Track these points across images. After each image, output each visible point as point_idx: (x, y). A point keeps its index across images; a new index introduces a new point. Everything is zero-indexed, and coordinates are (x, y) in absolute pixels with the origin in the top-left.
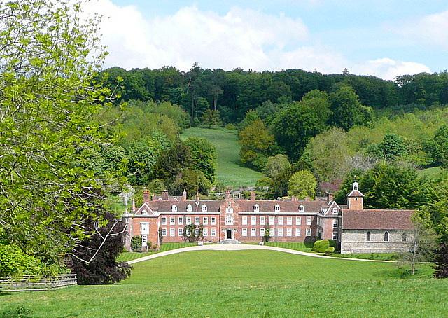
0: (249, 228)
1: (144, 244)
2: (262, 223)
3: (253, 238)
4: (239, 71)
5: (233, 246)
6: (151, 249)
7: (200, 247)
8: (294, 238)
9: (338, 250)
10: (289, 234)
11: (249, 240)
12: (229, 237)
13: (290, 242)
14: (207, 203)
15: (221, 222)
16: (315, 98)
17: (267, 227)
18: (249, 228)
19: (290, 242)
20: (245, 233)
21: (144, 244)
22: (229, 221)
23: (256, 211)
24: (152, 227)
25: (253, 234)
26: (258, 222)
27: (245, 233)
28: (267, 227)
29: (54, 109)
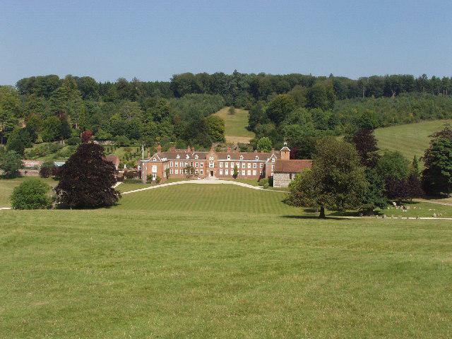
0: (224, 169)
1: (154, 179)
2: (232, 167)
3: (226, 176)
4: (262, 75)
5: (212, 180)
6: (158, 182)
7: (199, 181)
8: (252, 176)
9: (271, 184)
10: (249, 174)
11: (223, 177)
12: (212, 175)
13: (248, 180)
14: (198, 154)
15: (206, 165)
16: (299, 90)
17: (235, 169)
18: (224, 169)
19: (248, 180)
20: (221, 173)
21: (154, 179)
22: (212, 165)
23: (241, 160)
24: (160, 168)
25: (227, 173)
26: (229, 166)
27: (221, 173)
28: (235, 169)
29: (53, 324)
